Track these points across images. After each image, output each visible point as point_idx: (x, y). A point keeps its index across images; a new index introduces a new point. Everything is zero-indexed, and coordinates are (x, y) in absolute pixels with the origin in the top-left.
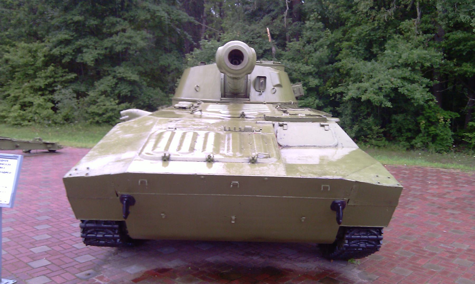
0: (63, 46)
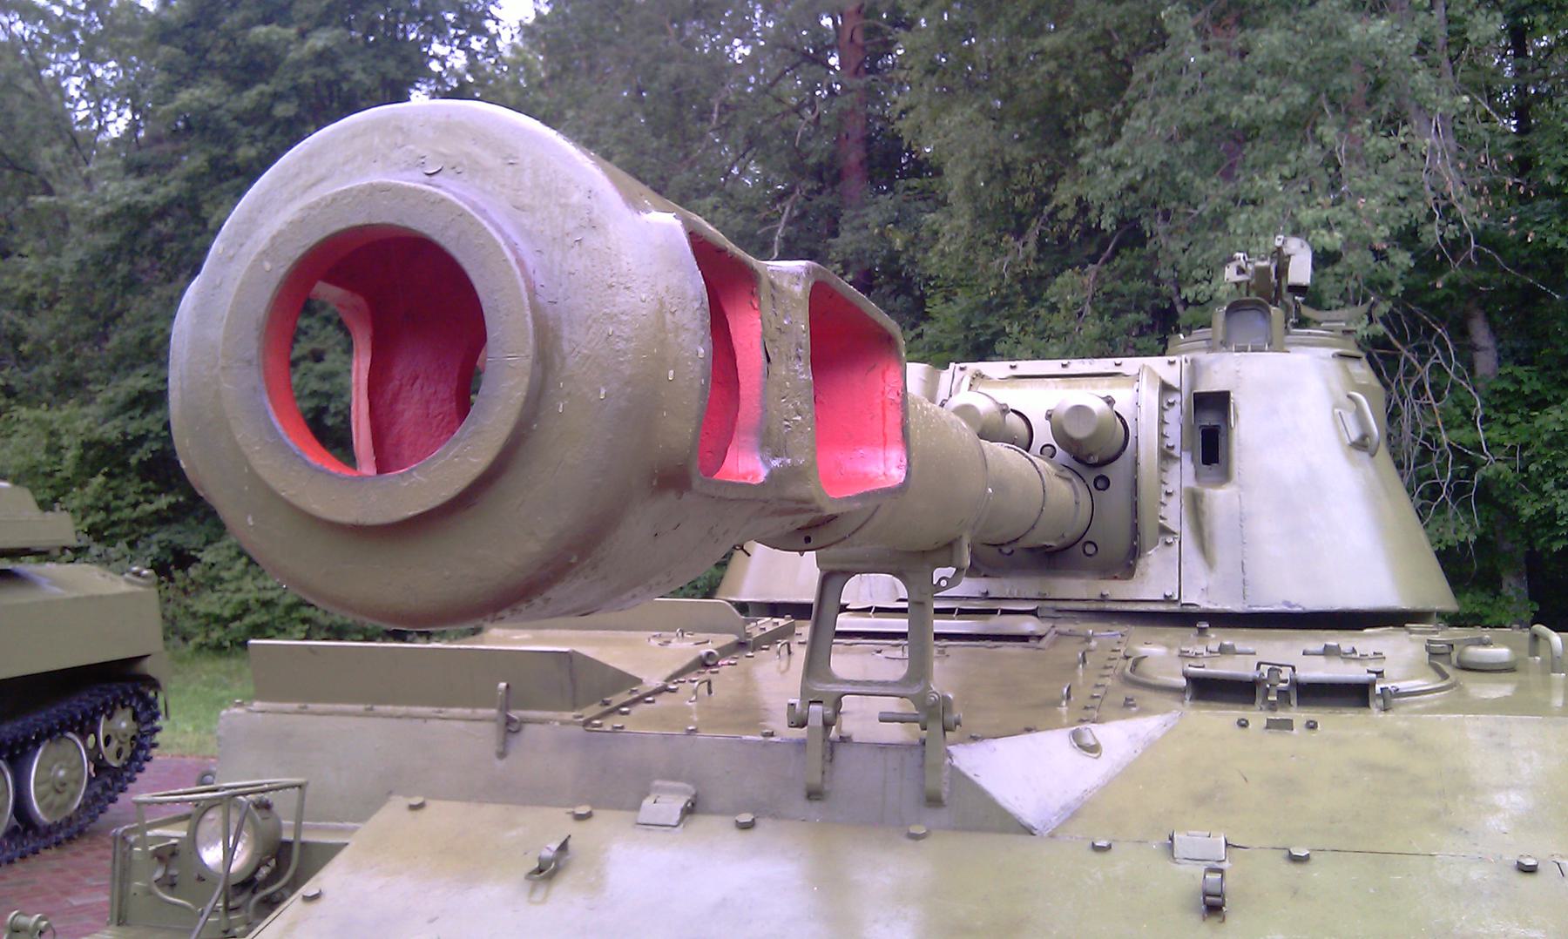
0: (138, 412)
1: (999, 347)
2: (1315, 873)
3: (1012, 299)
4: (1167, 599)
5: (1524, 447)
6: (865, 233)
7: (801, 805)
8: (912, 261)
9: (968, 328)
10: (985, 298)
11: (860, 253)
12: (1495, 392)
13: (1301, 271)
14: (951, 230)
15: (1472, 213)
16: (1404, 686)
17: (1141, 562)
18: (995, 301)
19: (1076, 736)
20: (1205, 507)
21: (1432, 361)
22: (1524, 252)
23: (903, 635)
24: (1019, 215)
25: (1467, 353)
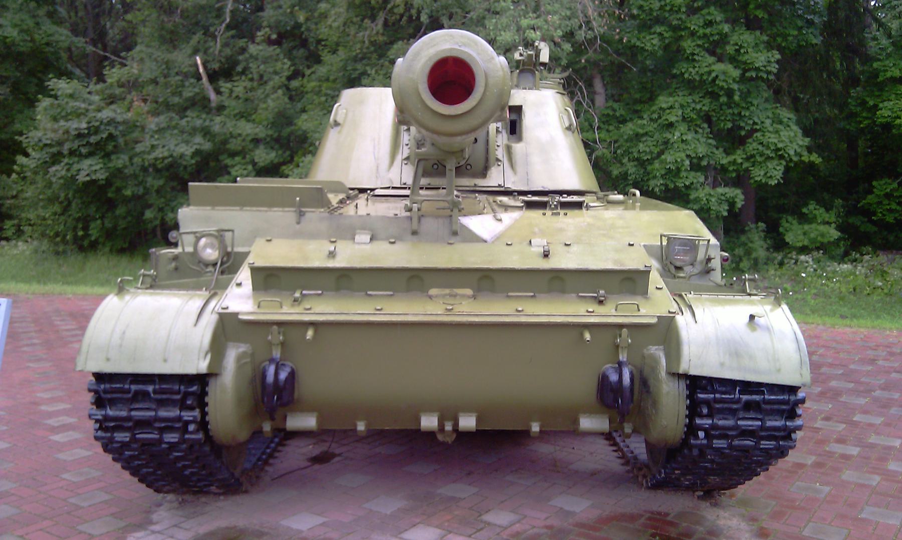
1: (364, 81)
2: (574, 248)
3: (369, 55)
4: (500, 186)
5: (615, 142)
6: (281, 11)
7: (410, 237)
8: (308, 30)
9: (345, 70)
10: (354, 54)
11: (278, 22)
12: (604, 115)
13: (545, 57)
14: (335, 14)
15: (599, 26)
16: (592, 204)
17: (489, 172)
18: (360, 56)
19: (495, 216)
20: (513, 151)
21: (576, 98)
22: (620, 47)
23: (408, 196)
24: (373, 8)
25: (592, 94)
